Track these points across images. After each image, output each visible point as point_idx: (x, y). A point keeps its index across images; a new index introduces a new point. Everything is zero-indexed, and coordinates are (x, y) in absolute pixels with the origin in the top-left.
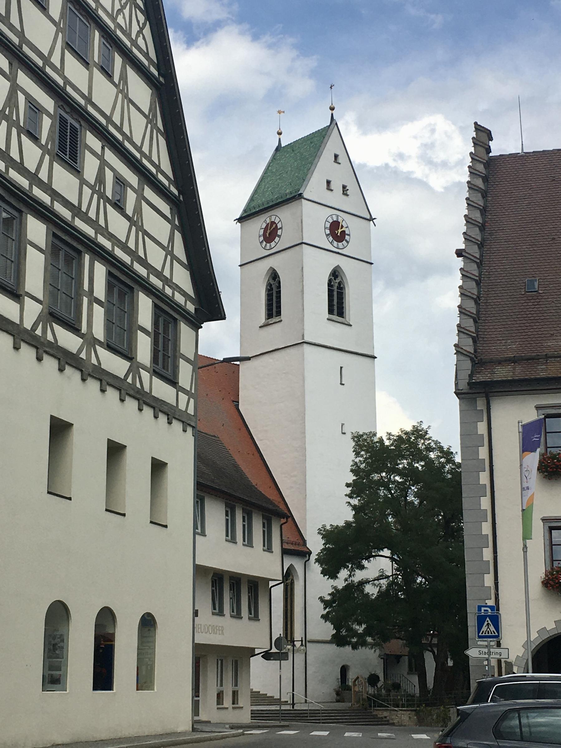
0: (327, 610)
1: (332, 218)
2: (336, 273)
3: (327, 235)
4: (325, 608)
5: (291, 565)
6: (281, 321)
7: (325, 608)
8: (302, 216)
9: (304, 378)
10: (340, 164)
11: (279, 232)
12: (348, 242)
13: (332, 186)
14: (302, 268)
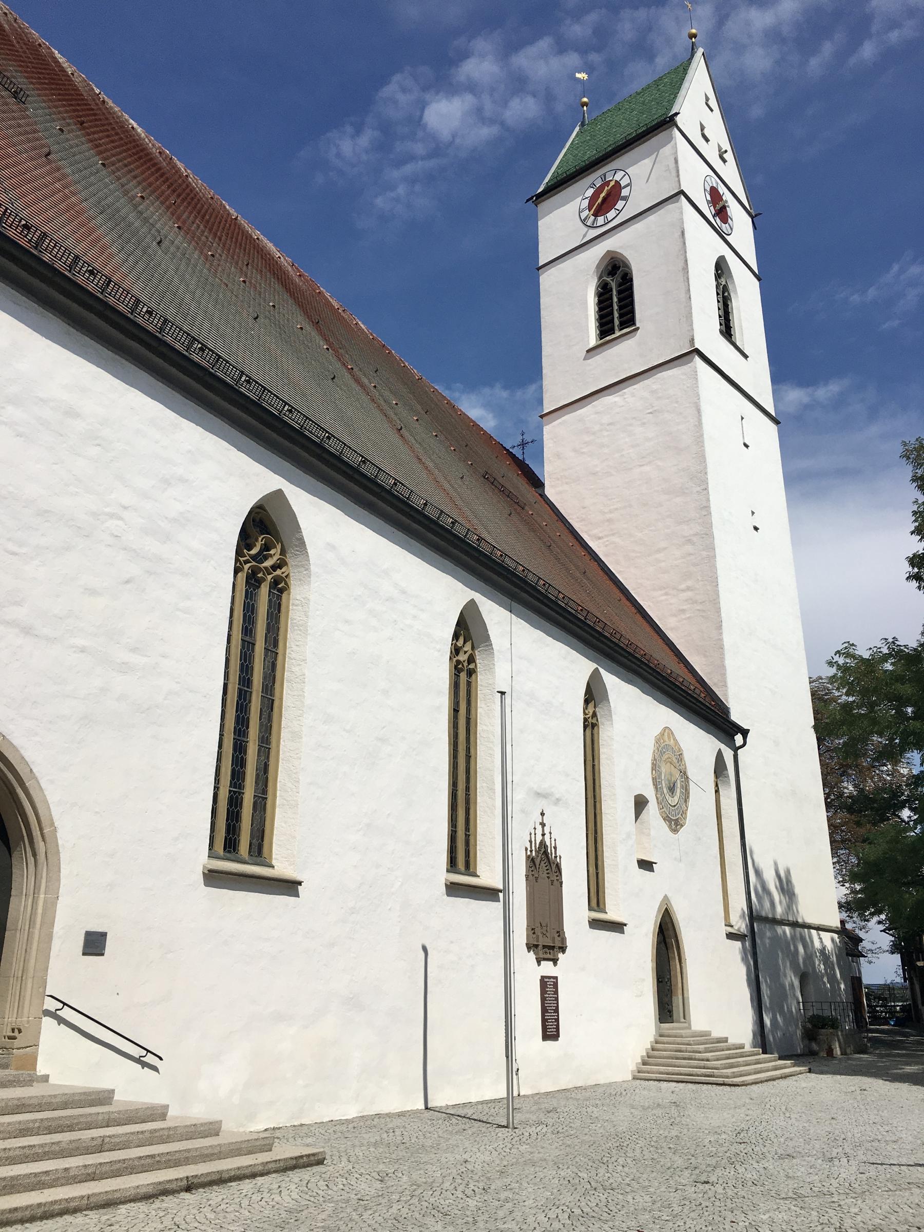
6: (638, 328)
11: (624, 192)
14: (683, 233)
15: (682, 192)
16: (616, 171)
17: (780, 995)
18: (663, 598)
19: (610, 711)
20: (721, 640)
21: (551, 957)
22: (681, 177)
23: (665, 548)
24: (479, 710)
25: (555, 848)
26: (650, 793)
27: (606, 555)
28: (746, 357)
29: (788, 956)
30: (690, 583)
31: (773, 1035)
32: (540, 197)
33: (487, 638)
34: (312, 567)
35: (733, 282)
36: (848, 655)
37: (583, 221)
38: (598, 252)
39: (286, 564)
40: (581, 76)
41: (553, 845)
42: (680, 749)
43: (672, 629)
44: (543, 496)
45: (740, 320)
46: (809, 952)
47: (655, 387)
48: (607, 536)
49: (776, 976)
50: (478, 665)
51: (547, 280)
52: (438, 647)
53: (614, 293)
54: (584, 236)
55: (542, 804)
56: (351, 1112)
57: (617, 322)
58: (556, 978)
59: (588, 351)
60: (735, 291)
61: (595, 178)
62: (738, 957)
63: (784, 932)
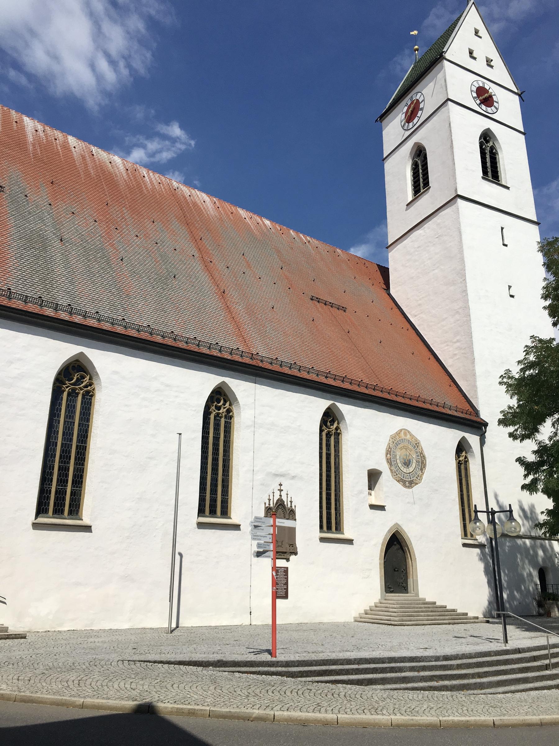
0: (531, 477)
1: (478, 83)
2: (486, 137)
3: (474, 98)
4: (526, 476)
5: (463, 438)
6: (430, 187)
7: (526, 476)
8: (445, 76)
9: (460, 232)
10: (481, 37)
11: (421, 106)
12: (497, 109)
13: (475, 55)
14: (450, 124)
15: (449, 100)
16: (417, 93)
17: (518, 581)
18: (446, 348)
19: (346, 425)
20: (474, 370)
21: (285, 557)
22: (448, 90)
23: (446, 318)
24: (235, 436)
25: (291, 502)
26: (384, 467)
27: (419, 326)
28: (508, 188)
29: (527, 557)
30: (458, 338)
31: (510, 604)
32: (383, 117)
33: (236, 399)
34: (102, 384)
35: (499, 143)
36: (509, 378)
37: (403, 127)
38: (410, 144)
39: (93, 384)
40: (415, 32)
41: (289, 500)
42: (416, 440)
43: (450, 366)
44: (389, 294)
45: (504, 165)
46: (548, 554)
47: (438, 221)
48: (419, 314)
49: (514, 567)
50: (235, 413)
51: (388, 166)
52: (194, 409)
53: (420, 167)
54: (403, 135)
55: (279, 480)
56: (126, 626)
57: (422, 185)
58: (287, 568)
59: (407, 205)
60: (500, 148)
61: (407, 100)
62: (477, 558)
63: (524, 543)
